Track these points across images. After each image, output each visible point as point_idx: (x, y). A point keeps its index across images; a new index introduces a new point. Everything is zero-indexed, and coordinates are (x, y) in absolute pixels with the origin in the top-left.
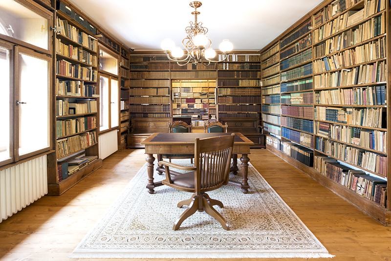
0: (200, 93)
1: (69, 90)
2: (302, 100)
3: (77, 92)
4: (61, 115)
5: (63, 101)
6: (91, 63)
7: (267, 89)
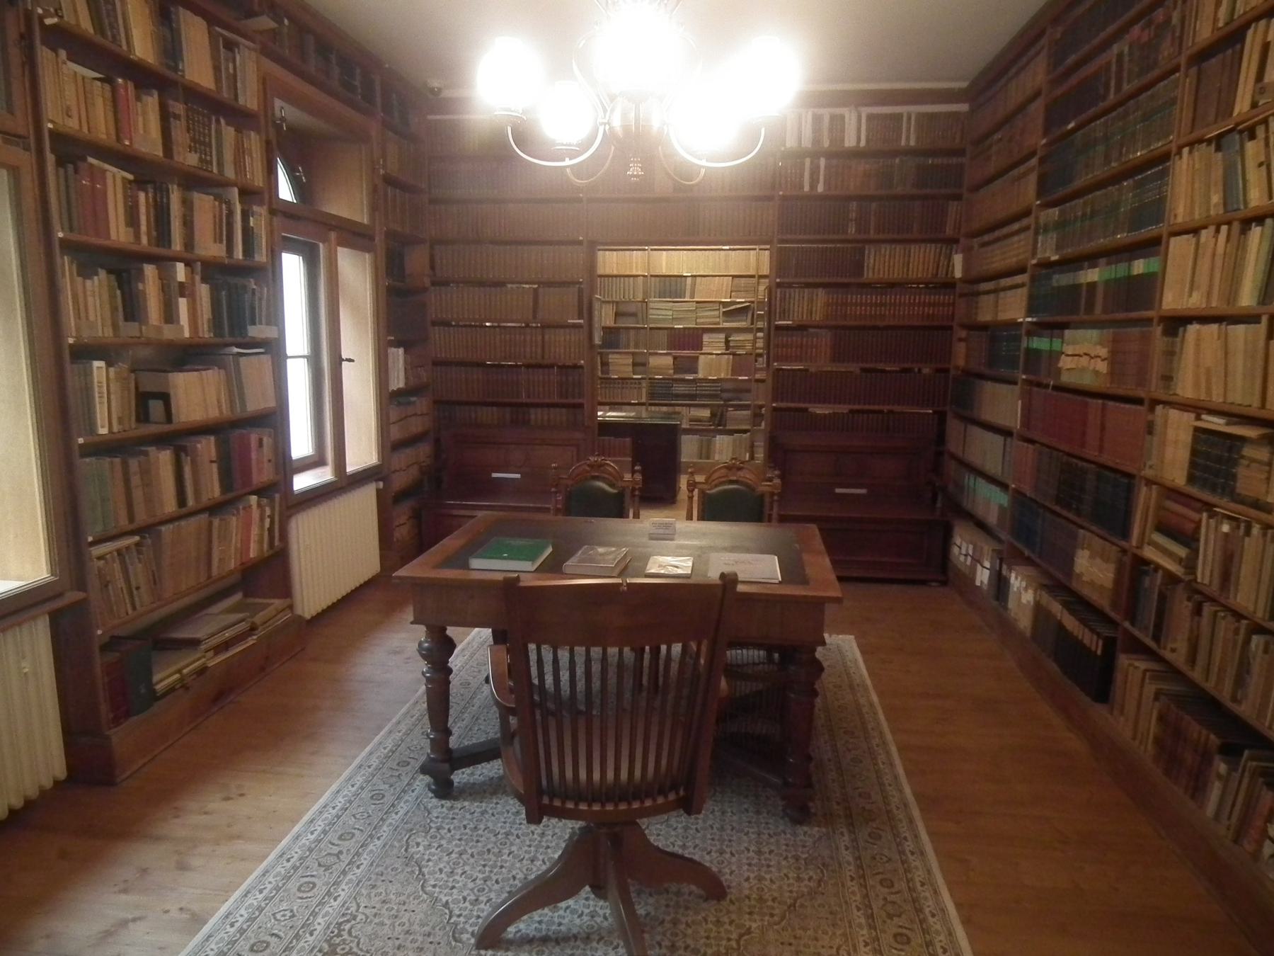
0: (725, 304)
1: (132, 308)
2: (1102, 367)
3: (170, 315)
4: (103, 431)
5: (109, 364)
6: (230, 173)
7: (979, 294)
